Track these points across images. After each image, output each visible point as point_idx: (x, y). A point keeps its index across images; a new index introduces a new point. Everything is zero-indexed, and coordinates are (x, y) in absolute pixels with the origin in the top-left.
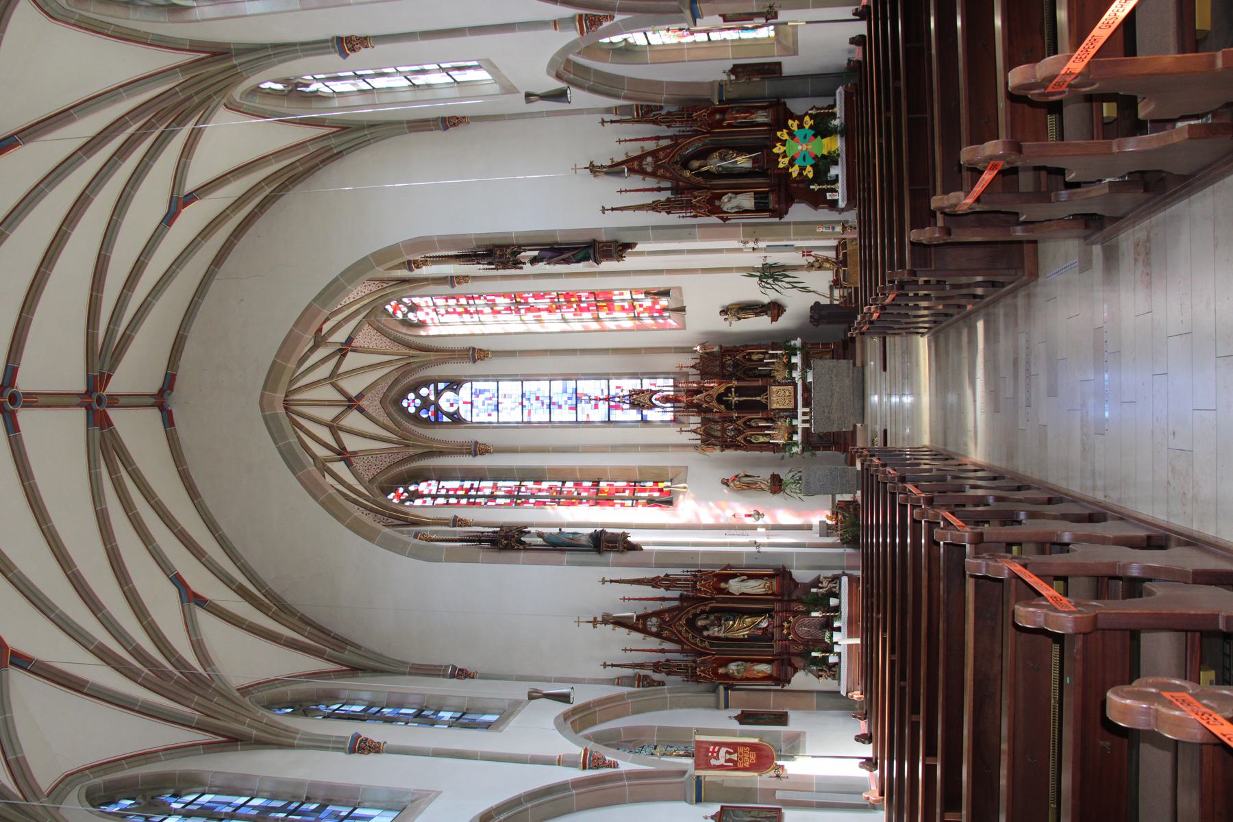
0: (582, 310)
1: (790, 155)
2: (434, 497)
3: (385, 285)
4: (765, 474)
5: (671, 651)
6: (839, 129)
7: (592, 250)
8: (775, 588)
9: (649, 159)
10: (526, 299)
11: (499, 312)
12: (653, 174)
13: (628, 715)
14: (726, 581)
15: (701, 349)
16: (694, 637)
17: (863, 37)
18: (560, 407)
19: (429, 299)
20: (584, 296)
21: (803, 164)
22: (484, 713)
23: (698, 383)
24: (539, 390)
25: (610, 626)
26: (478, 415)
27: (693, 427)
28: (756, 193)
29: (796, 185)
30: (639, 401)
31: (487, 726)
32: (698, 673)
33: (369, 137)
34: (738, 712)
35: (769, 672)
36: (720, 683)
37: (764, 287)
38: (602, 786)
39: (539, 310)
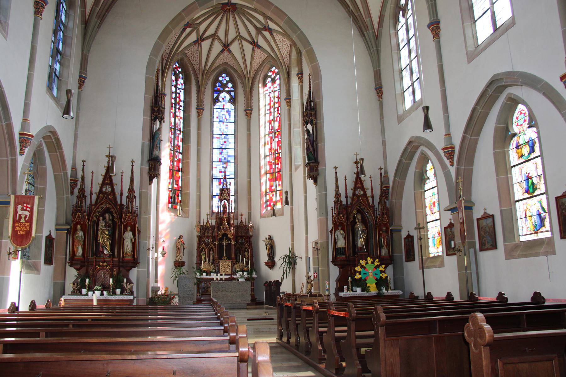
0: (271, 166)
1: (366, 266)
2: (176, 86)
3: (287, 65)
4: (184, 258)
5: (91, 199)
6: (381, 292)
7: (314, 162)
8: (127, 258)
9: (362, 193)
10: (277, 137)
11: (270, 123)
12: (354, 194)
13: (54, 172)
14: (131, 230)
15: (251, 226)
16: (99, 212)
17: (453, 299)
18: (221, 153)
19: (278, 88)
20: (279, 166)
21: (362, 273)
22: (58, 89)
23: (233, 224)
24: (230, 143)
25: (107, 161)
26: (217, 111)
27: (210, 221)
28: (345, 248)
29: (349, 270)
30: (224, 194)
31: (50, 88)
32: (78, 214)
33: (372, 50)
34: (54, 236)
35: (77, 254)
36: (71, 227)
37: (284, 258)
38: (7, 142)
39: (271, 144)
